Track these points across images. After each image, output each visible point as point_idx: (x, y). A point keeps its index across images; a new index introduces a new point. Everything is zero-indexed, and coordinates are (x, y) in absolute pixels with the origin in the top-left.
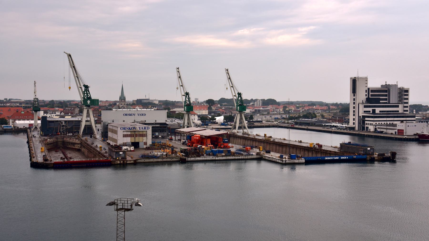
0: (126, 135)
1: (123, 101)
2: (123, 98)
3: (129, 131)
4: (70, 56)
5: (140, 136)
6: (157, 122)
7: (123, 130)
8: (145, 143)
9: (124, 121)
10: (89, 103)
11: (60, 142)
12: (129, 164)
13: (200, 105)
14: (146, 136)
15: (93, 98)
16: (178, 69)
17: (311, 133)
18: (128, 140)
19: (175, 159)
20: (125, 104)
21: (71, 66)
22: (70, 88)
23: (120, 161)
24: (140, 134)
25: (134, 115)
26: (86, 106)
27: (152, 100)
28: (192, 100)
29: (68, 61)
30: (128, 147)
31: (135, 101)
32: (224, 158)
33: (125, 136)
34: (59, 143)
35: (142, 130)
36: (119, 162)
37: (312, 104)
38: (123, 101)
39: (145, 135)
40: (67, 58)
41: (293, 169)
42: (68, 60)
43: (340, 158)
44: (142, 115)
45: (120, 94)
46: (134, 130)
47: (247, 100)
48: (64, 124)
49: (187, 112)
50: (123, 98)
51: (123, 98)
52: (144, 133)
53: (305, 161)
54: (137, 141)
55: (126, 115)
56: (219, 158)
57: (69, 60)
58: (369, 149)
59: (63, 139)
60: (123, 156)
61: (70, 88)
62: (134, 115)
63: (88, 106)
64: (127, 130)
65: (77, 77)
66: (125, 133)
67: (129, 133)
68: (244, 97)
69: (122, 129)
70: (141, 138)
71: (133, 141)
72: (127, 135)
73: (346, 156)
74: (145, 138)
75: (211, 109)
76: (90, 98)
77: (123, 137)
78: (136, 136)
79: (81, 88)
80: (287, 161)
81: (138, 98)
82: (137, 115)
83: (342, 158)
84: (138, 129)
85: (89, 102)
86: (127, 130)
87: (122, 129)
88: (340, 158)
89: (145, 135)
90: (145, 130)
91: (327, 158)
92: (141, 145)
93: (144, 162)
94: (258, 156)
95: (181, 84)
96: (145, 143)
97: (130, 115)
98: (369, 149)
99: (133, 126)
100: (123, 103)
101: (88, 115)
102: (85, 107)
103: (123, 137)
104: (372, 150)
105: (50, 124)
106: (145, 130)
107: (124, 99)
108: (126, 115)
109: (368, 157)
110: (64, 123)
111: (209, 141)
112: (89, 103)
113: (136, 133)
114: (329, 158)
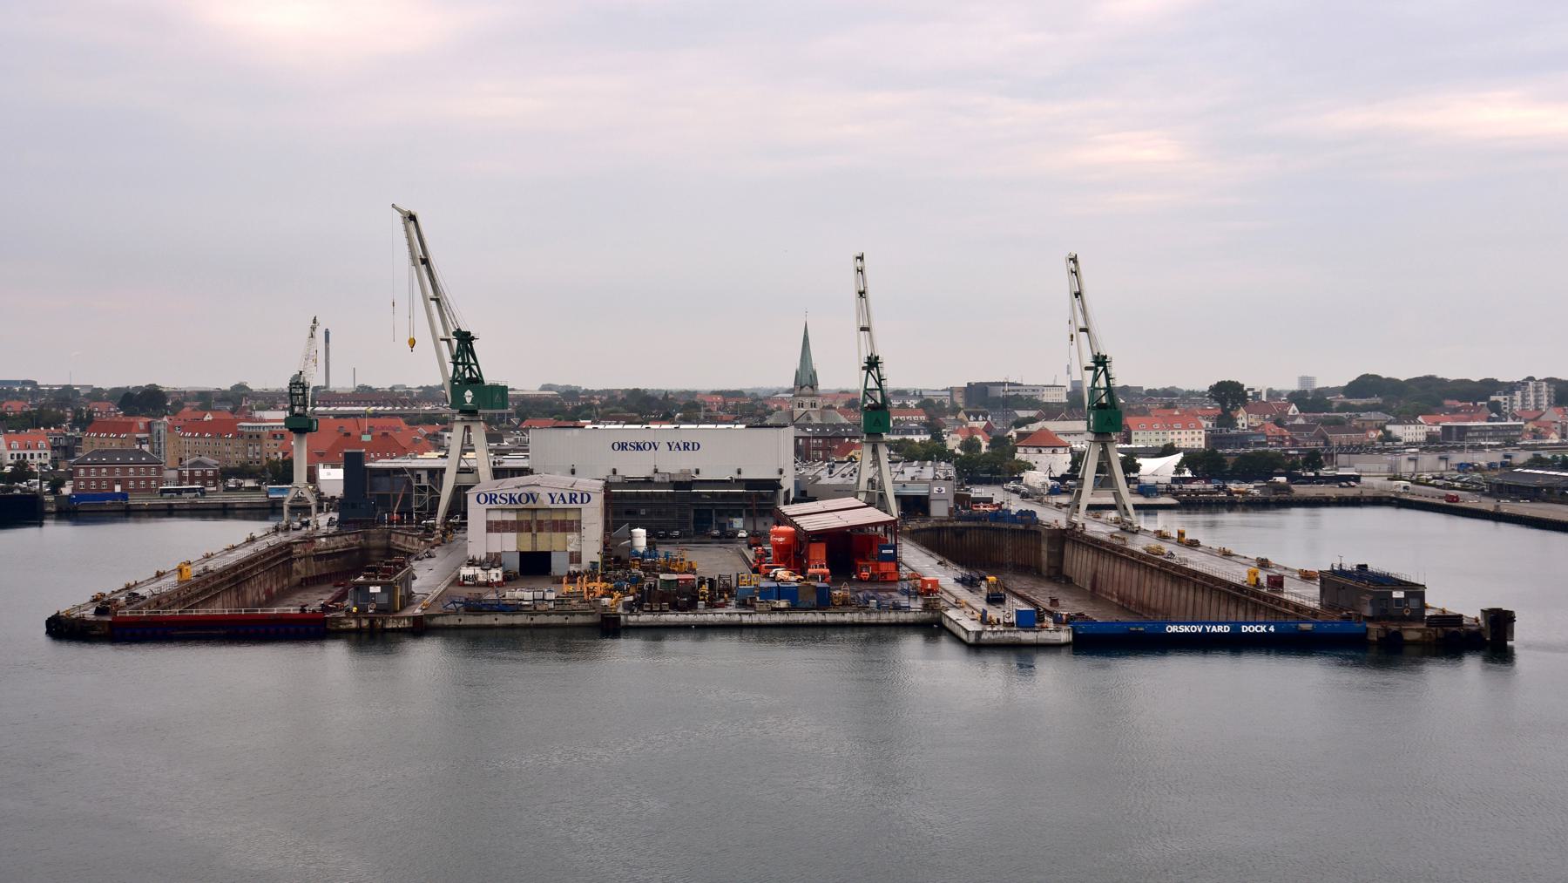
0: (497, 523)
1: (807, 390)
2: (806, 380)
3: (510, 510)
4: (413, 218)
5: (555, 530)
6: (743, 476)
7: (487, 505)
8: (575, 558)
9: (573, 472)
10: (469, 400)
11: (375, 548)
12: (393, 630)
13: (1169, 402)
14: (579, 529)
15: (489, 379)
16: (861, 258)
17: (1244, 525)
18: (509, 544)
19: (579, 619)
20: (813, 405)
21: (413, 257)
22: (412, 343)
23: (359, 622)
24: (555, 522)
25: (653, 446)
26: (461, 412)
27: (1035, 389)
28: (891, 384)
29: (405, 242)
30: (478, 570)
31: (959, 390)
32: (778, 618)
33: (493, 527)
34: (375, 553)
35: (561, 505)
36: (354, 624)
37: (695, 393)
38: (807, 390)
39: (572, 526)
40: (402, 227)
41: (1026, 667)
42: (404, 234)
43: (1236, 625)
44: (686, 447)
45: (795, 363)
46: (531, 505)
47: (1379, 378)
48: (425, 481)
49: (1097, 434)
50: (806, 380)
51: (806, 380)
52: (571, 516)
53: (1075, 635)
54: (542, 547)
55: (623, 446)
56: (755, 619)
57: (409, 237)
58: (1398, 594)
59: (389, 537)
60: (384, 600)
61: (412, 343)
62: (653, 446)
63: (470, 413)
64: (501, 503)
65: (437, 300)
66: (496, 517)
67: (512, 517)
68: (1123, 376)
69: (482, 498)
70: (558, 536)
71: (528, 549)
72: (505, 523)
73: (1268, 625)
74: (572, 536)
75: (1232, 422)
76: (476, 382)
77: (489, 530)
78: (540, 530)
79: (448, 341)
80: (984, 636)
81: (974, 380)
82: (663, 447)
83: (1245, 629)
84: (547, 503)
85: (475, 398)
86: (501, 503)
87: (482, 498)
88: (1236, 625)
89: (572, 526)
90: (574, 505)
91: (1174, 629)
92: (559, 565)
93: (457, 628)
94: (928, 615)
95: (1083, 325)
96: (575, 558)
97: (638, 447)
98: (1398, 594)
99: (527, 490)
100: (807, 401)
101: (467, 447)
102: (458, 418)
103: (489, 530)
104: (1414, 603)
105: (377, 480)
106: (574, 505)
107: (813, 384)
108: (623, 446)
109: (1374, 631)
110: (424, 476)
111: (818, 552)
112: (469, 400)
113: (541, 516)
114: (1186, 629)
